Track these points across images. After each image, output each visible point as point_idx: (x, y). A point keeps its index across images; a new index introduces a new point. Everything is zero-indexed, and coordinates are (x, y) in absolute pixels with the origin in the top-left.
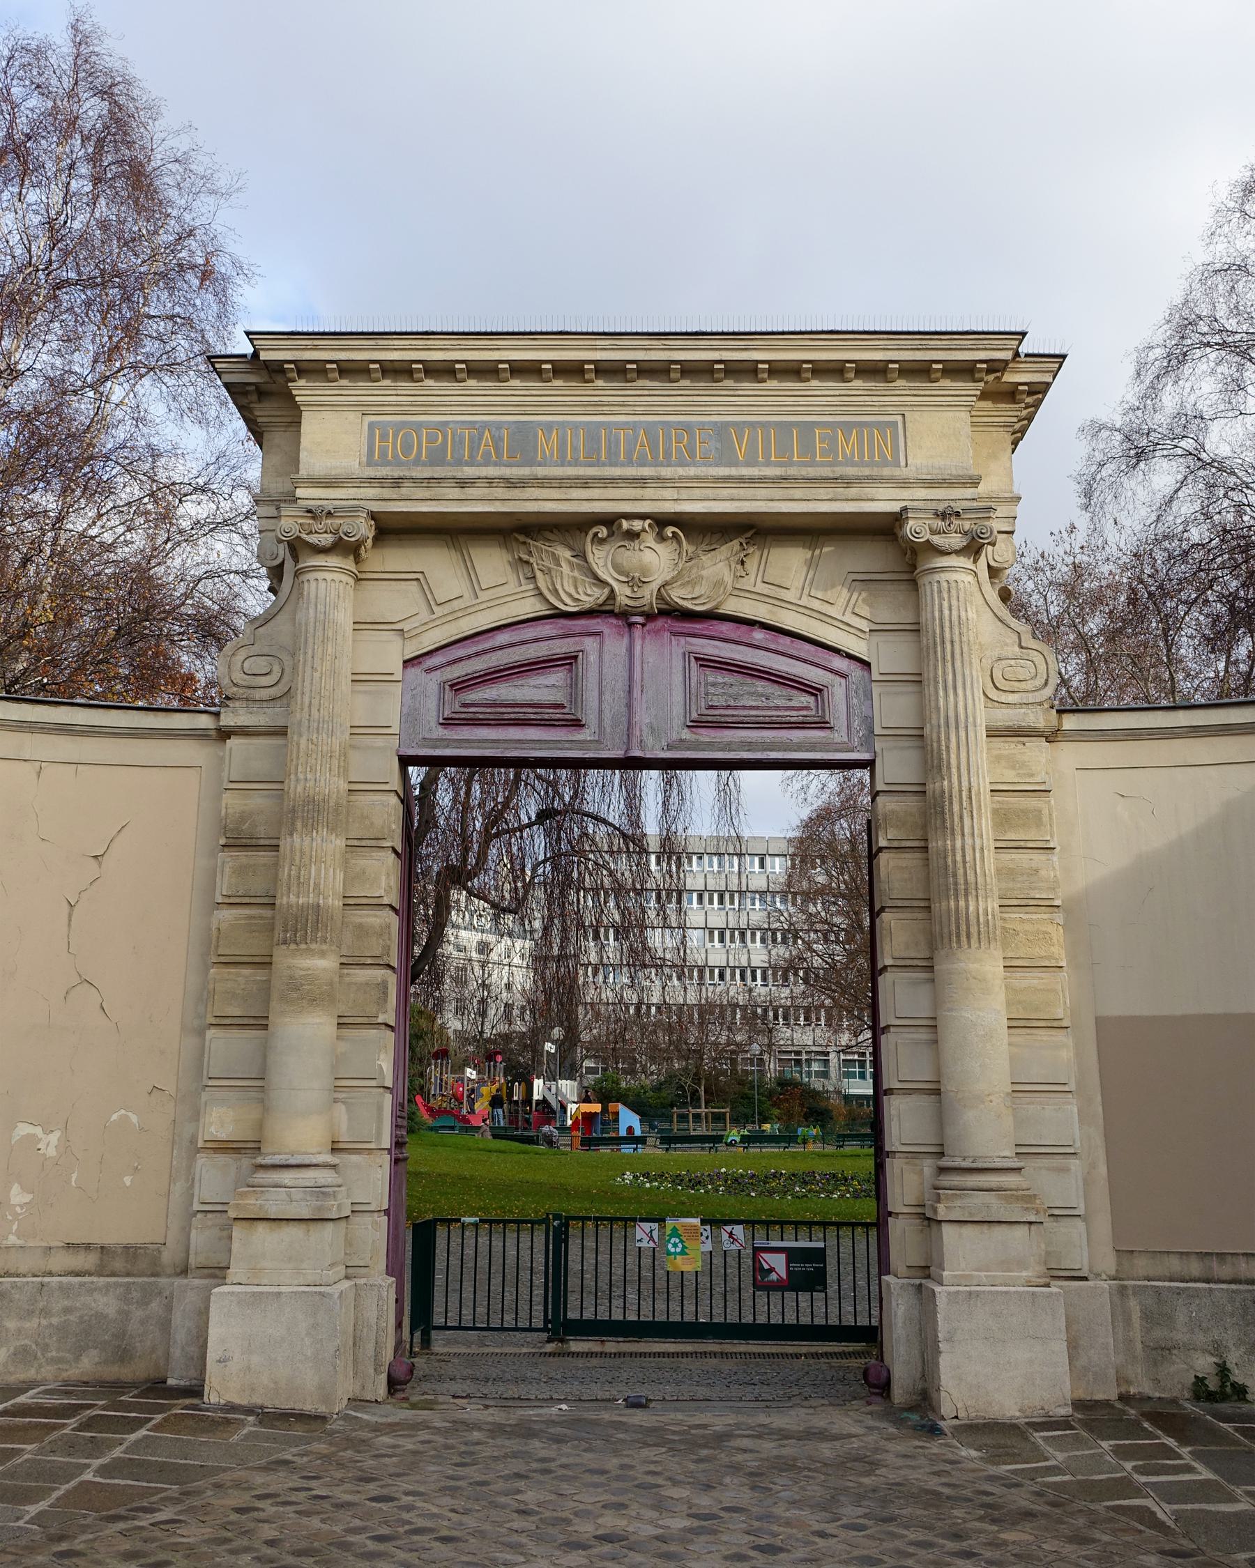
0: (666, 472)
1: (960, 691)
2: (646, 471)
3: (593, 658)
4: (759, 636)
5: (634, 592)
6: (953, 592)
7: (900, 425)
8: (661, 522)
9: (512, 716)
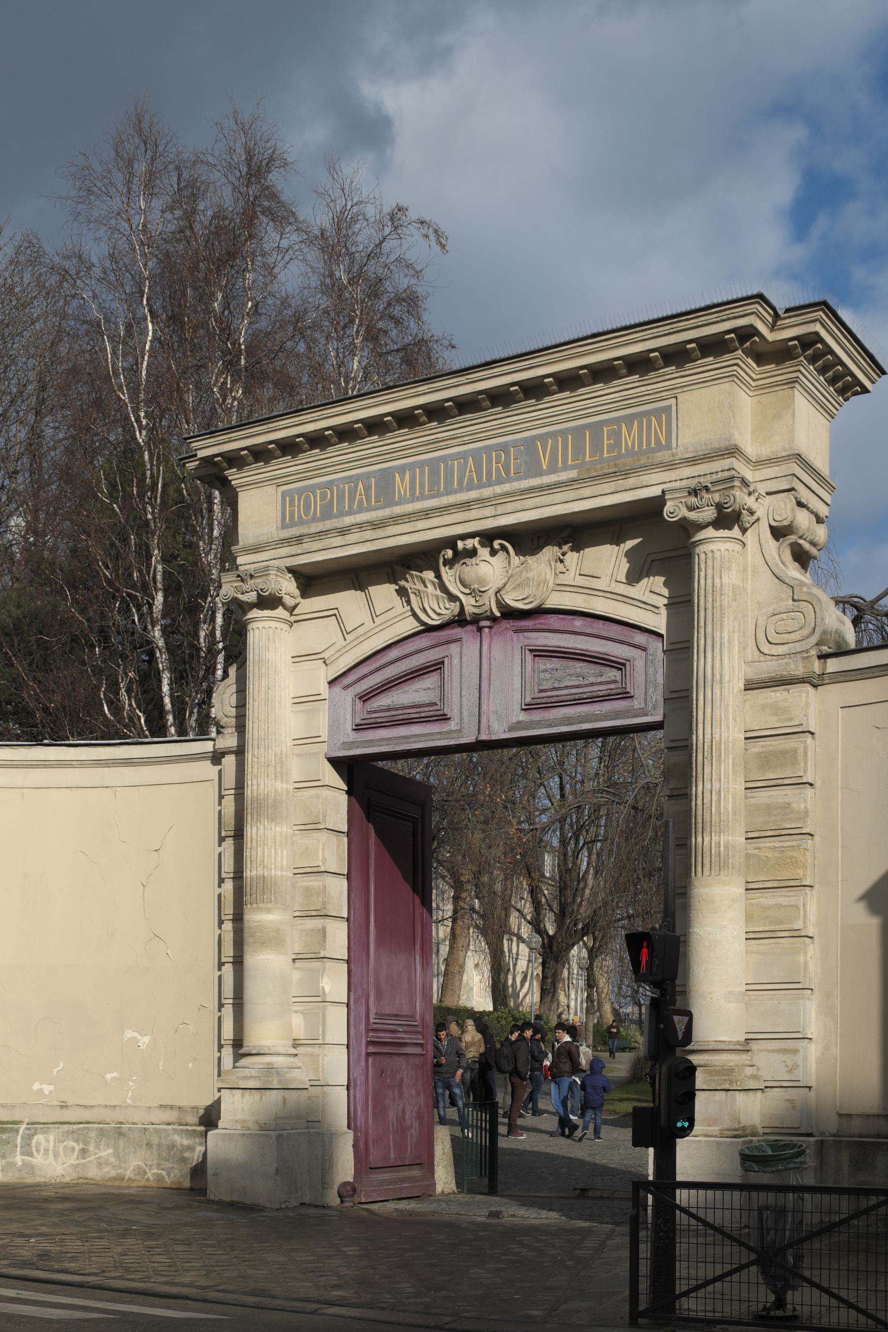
0: (487, 492)
1: (709, 655)
2: (473, 495)
3: (456, 661)
4: (578, 623)
5: (477, 601)
6: (710, 562)
7: (674, 408)
8: (488, 537)
9: (401, 717)
